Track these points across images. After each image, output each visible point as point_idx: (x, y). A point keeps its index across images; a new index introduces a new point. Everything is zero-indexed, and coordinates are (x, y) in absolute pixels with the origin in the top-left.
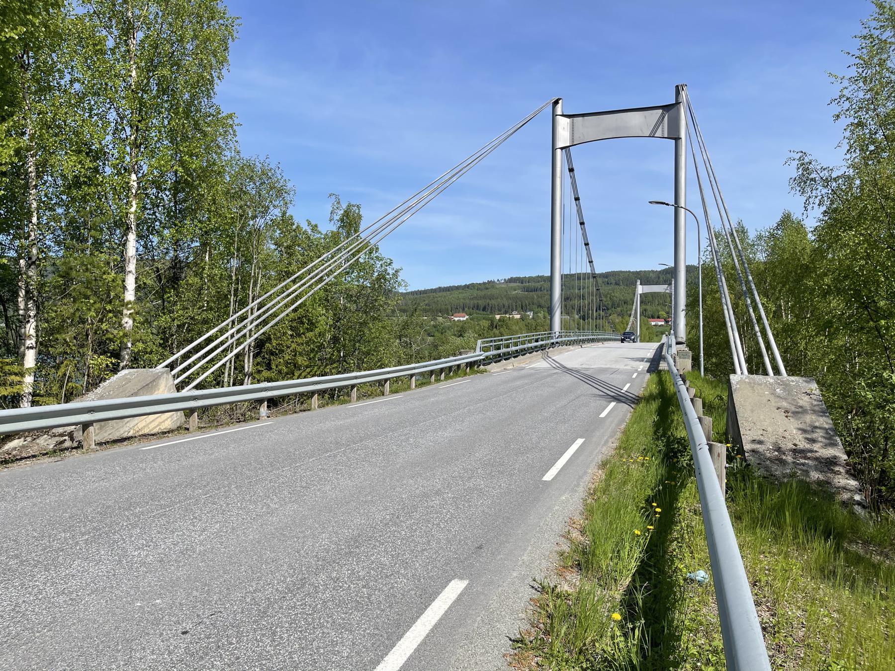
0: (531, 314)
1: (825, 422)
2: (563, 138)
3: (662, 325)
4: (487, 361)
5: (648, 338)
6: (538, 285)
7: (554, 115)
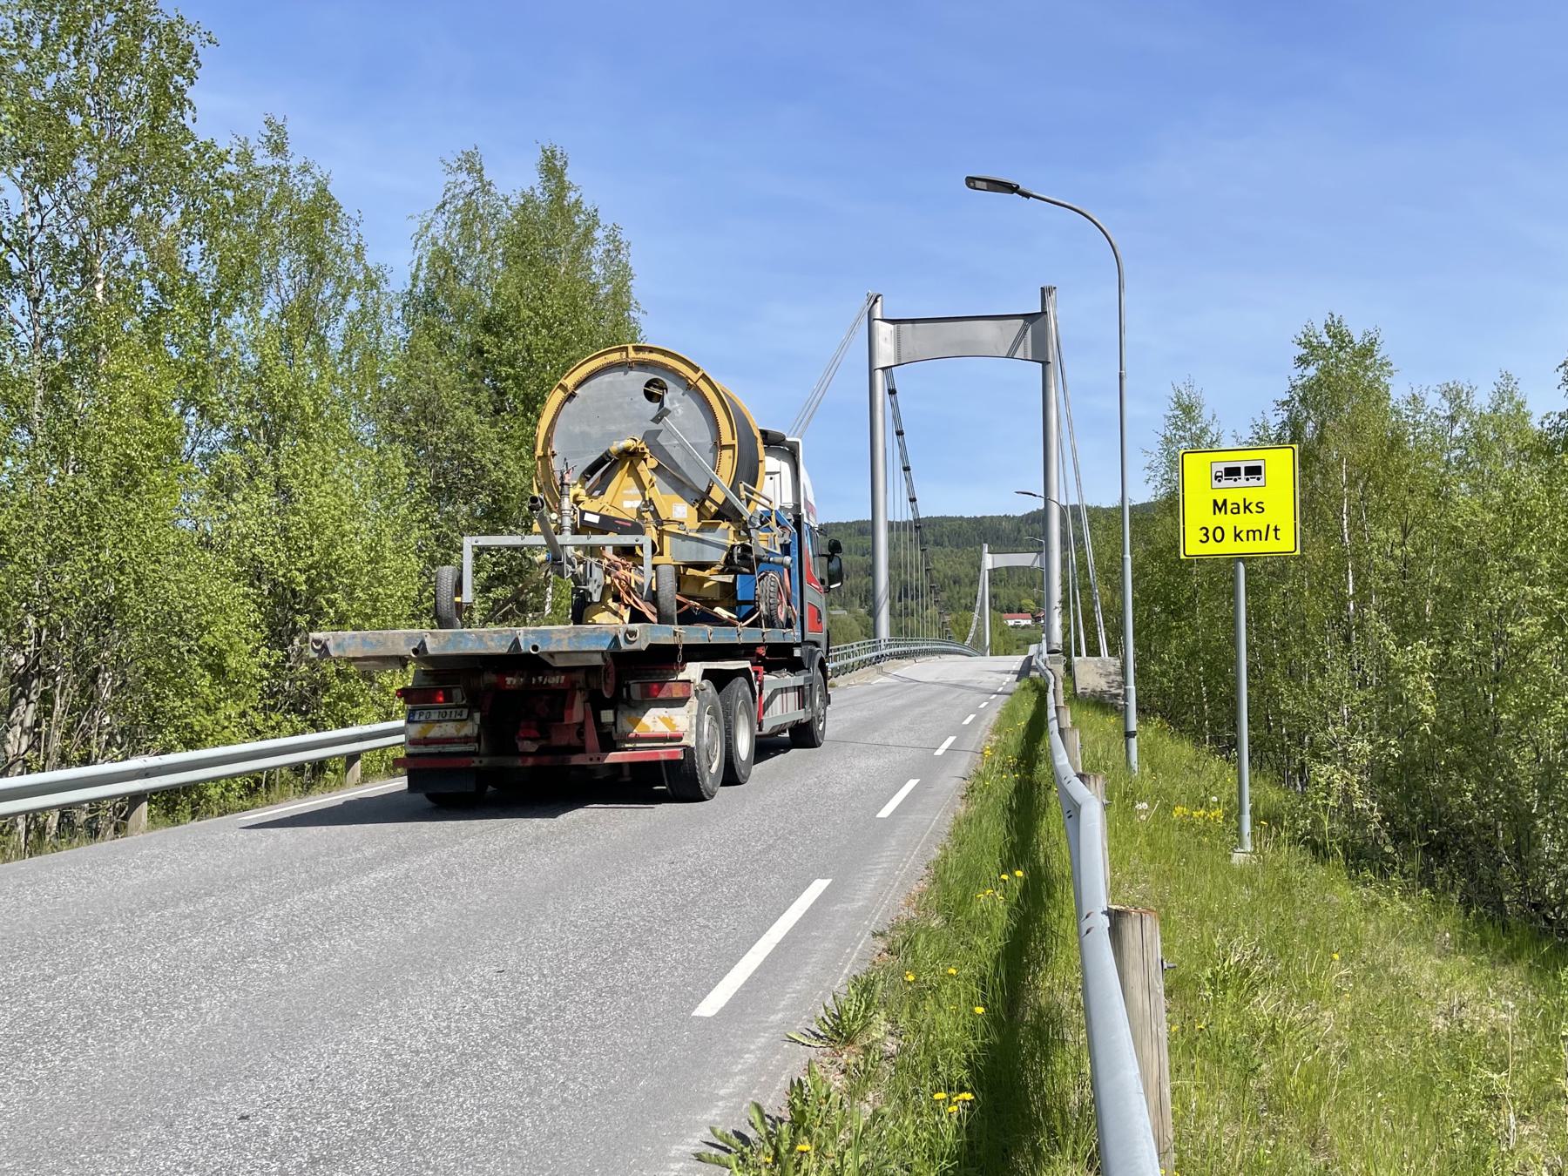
2: (886, 353)
5: (1007, 643)
7: (871, 320)
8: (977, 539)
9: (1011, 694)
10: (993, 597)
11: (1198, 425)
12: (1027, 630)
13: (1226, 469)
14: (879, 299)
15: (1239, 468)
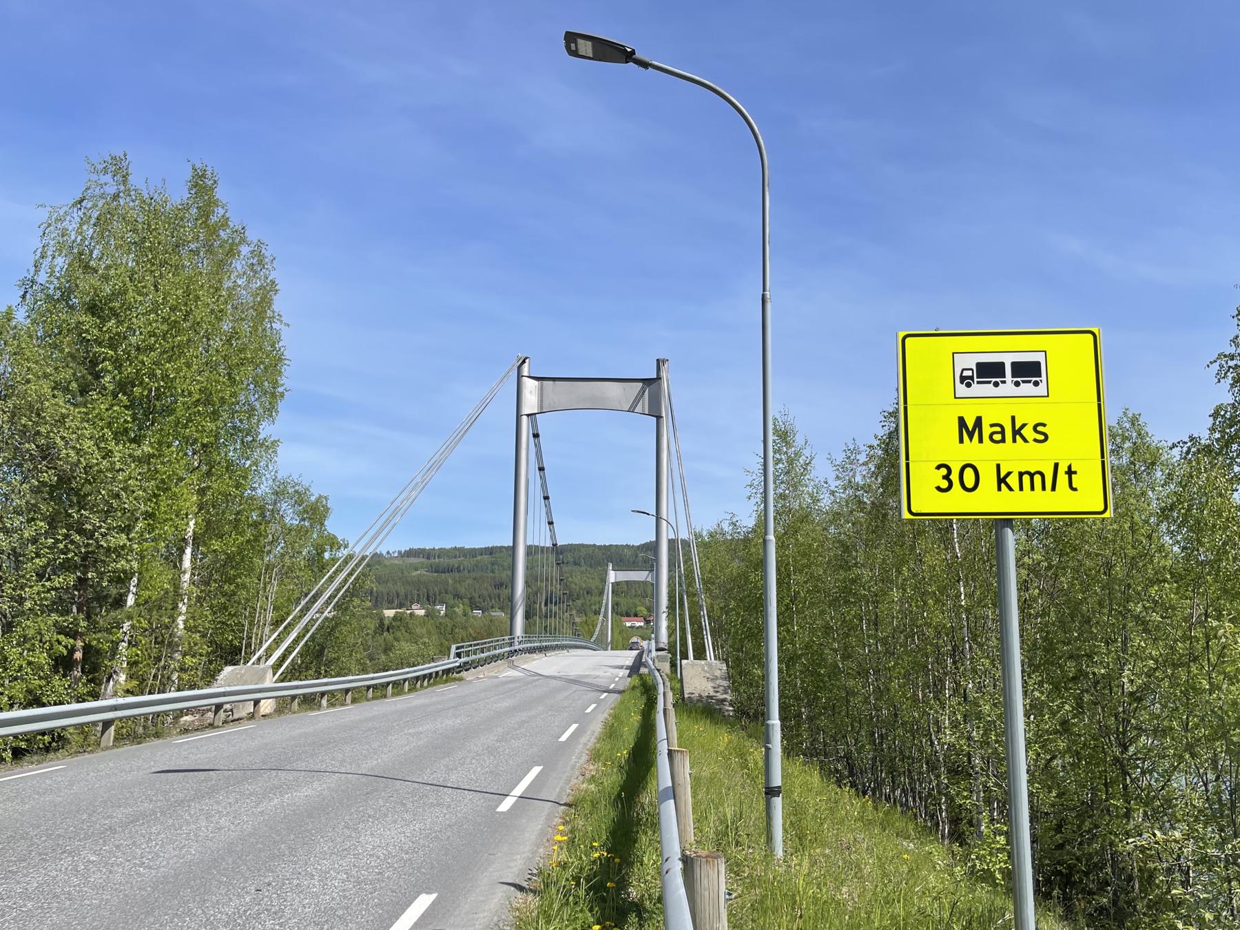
0: (442, 609)
1: (725, 683)
2: (531, 402)
3: (641, 627)
4: (465, 667)
6: (454, 562)
7: (520, 376)
9: (620, 692)
10: (616, 605)
11: (793, 449)
12: (640, 630)
13: (979, 365)
14: (527, 361)
15: (1002, 364)
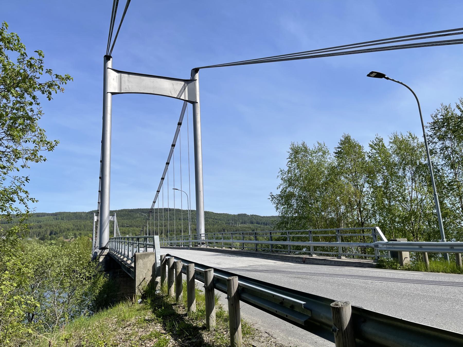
8: (74, 218)
